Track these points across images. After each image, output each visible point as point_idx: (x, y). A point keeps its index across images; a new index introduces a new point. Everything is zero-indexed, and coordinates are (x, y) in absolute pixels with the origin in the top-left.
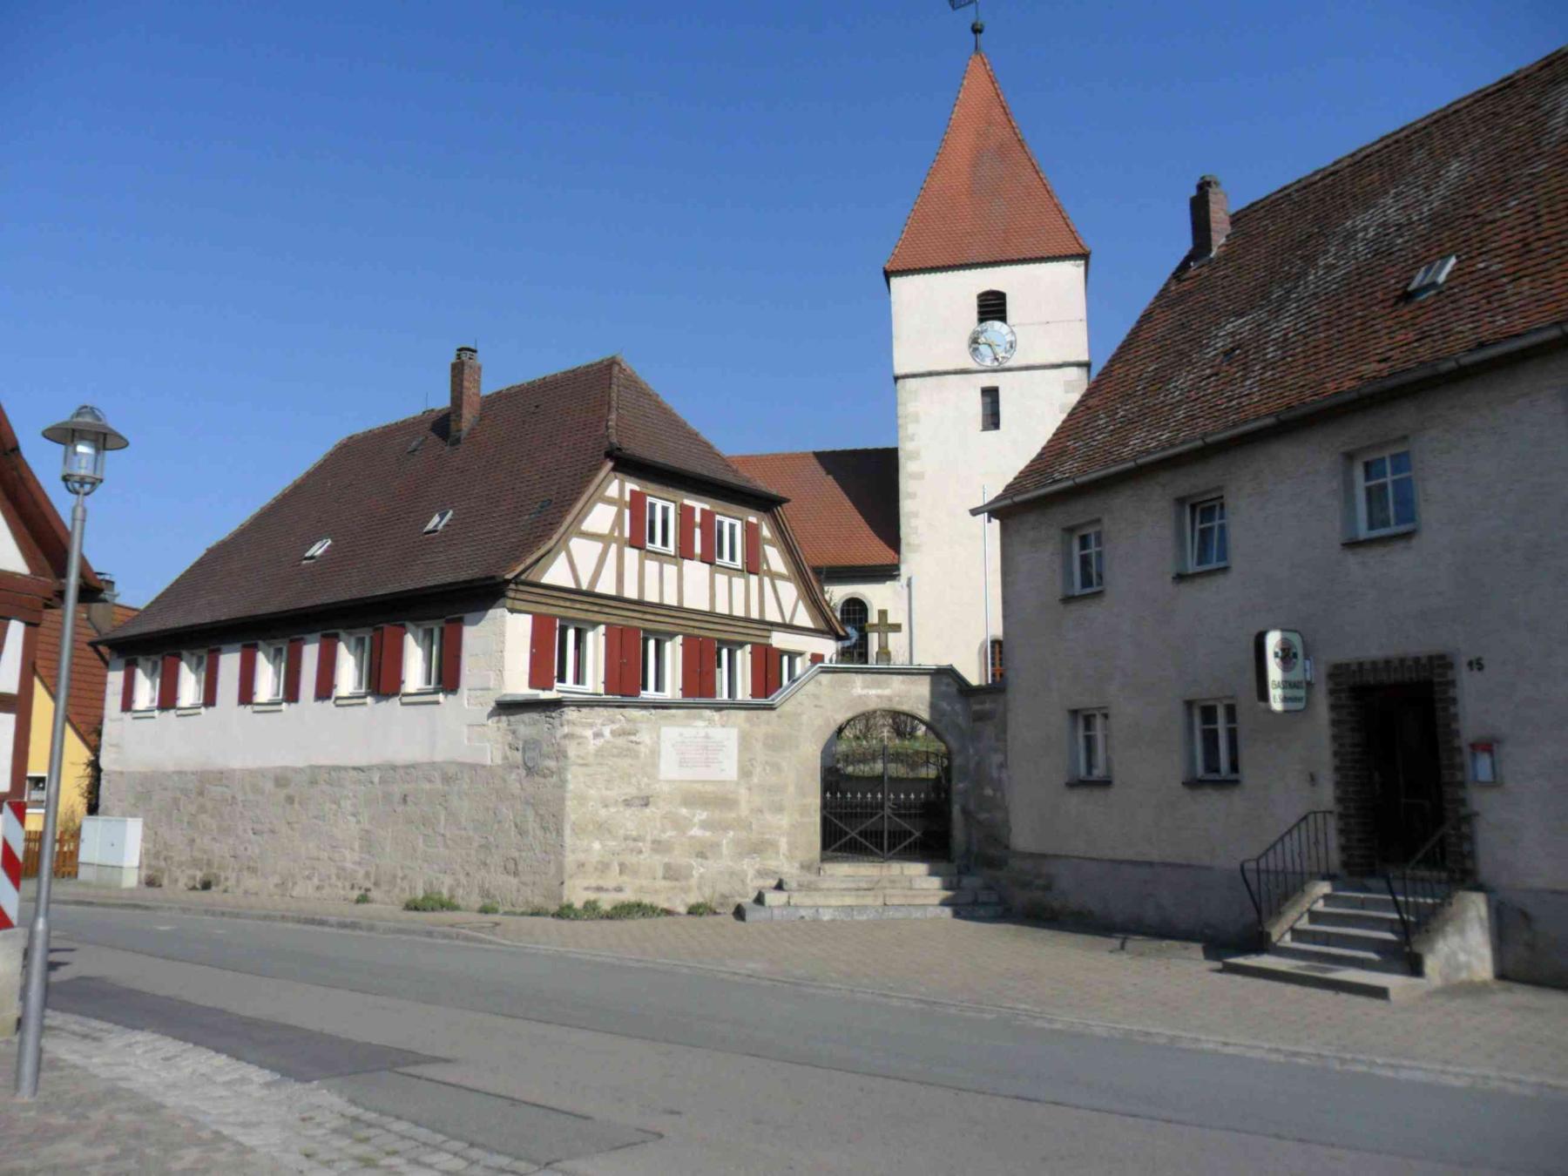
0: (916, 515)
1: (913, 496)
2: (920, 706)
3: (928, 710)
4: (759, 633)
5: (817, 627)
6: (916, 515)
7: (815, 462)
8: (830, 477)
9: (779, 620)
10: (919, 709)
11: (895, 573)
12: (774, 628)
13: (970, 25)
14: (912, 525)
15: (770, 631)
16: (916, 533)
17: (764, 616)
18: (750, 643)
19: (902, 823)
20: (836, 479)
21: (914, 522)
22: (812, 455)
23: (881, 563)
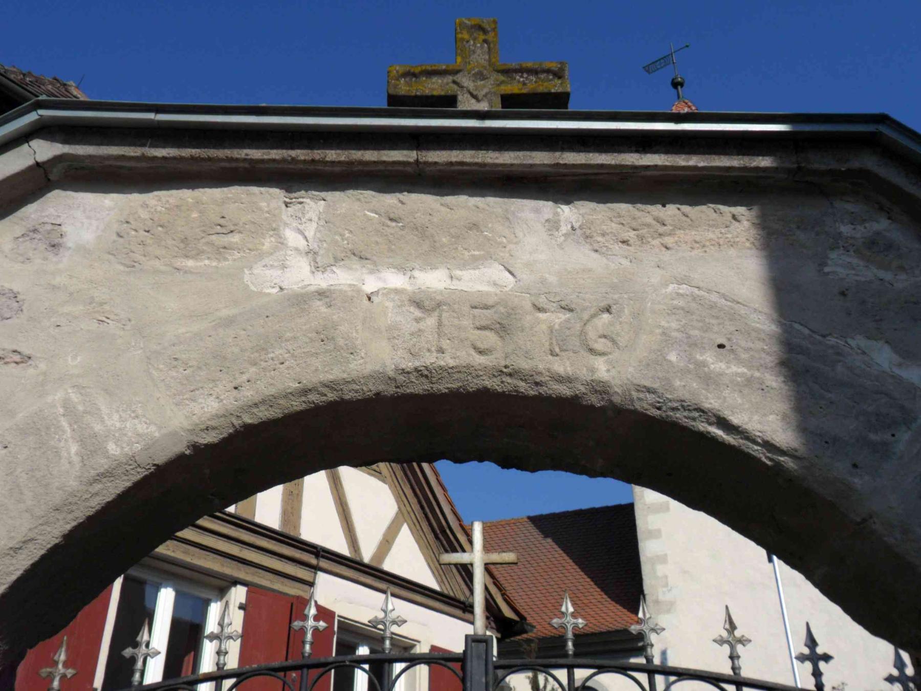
0: (663, 559)
1: (655, 534)
2: (715, 363)
3: (774, 381)
4: (290, 569)
5: (447, 591)
6: (663, 559)
7: (530, 527)
8: (549, 540)
9: (339, 545)
10: (709, 380)
11: (640, 644)
12: (324, 563)
13: (671, 80)
14: (660, 573)
15: (316, 568)
16: (666, 585)
17: (297, 526)
18: (244, 583)
19: (725, 436)
20: (557, 541)
21: (661, 570)
22: (527, 520)
23: (615, 628)
